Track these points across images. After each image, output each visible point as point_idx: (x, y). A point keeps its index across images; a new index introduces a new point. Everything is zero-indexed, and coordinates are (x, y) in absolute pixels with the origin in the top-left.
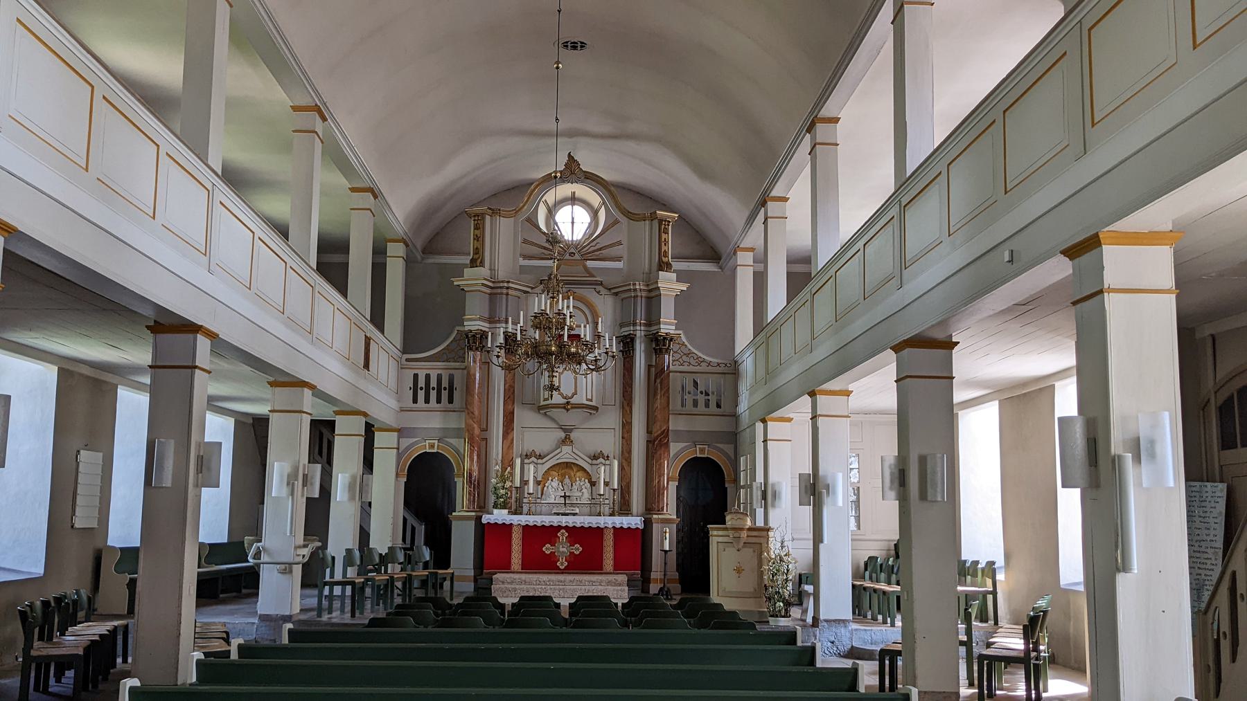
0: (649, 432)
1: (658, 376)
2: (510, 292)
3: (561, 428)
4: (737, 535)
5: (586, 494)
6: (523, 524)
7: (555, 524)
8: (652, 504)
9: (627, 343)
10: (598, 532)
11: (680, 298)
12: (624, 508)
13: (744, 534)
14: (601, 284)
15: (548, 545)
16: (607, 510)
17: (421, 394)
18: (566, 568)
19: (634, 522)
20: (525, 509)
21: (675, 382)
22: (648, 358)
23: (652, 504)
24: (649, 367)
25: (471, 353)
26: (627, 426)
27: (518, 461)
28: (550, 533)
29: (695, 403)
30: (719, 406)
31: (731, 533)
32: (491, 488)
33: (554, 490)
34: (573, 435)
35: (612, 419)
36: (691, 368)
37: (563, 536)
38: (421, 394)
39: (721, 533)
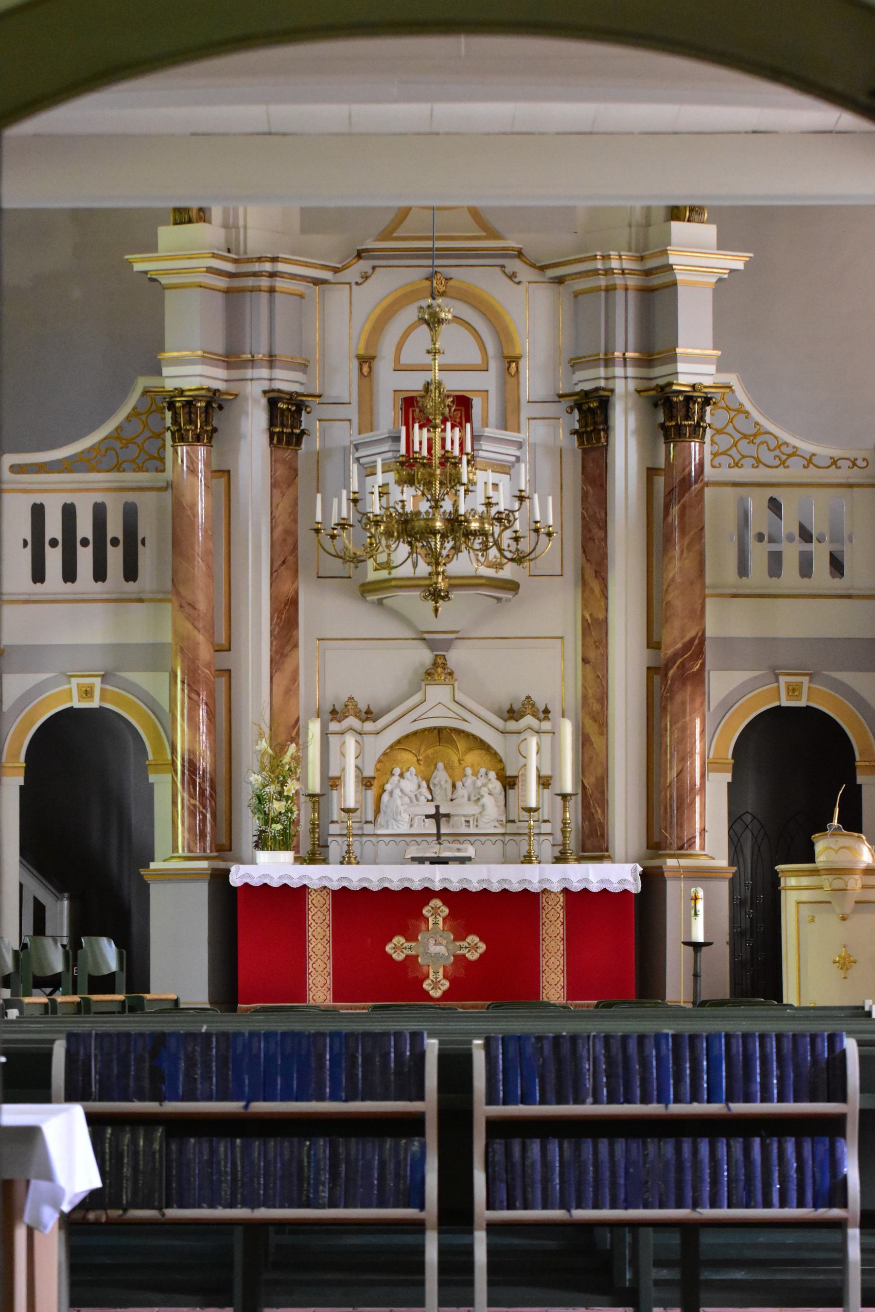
0: (653, 644)
1: (673, 498)
2: (279, 283)
3: (422, 638)
4: (838, 884)
5: (492, 808)
6: (335, 886)
7: (416, 886)
8: (664, 829)
9: (591, 414)
10: (527, 902)
11: (725, 287)
12: (594, 845)
13: (855, 882)
14: (520, 254)
15: (399, 940)
16: (546, 849)
17: (54, 558)
18: (446, 996)
19: (618, 875)
20: (335, 848)
21: (718, 509)
22: (647, 448)
23: (664, 829)
24: (651, 473)
25: (183, 450)
26: (595, 631)
27: (314, 728)
28: (401, 908)
29: (775, 562)
30: (837, 565)
31: (826, 881)
32: (245, 798)
33: (407, 801)
34: (455, 657)
35: (554, 610)
36: (736, 474)
37: (436, 913)
38: (54, 558)
39: (805, 881)
